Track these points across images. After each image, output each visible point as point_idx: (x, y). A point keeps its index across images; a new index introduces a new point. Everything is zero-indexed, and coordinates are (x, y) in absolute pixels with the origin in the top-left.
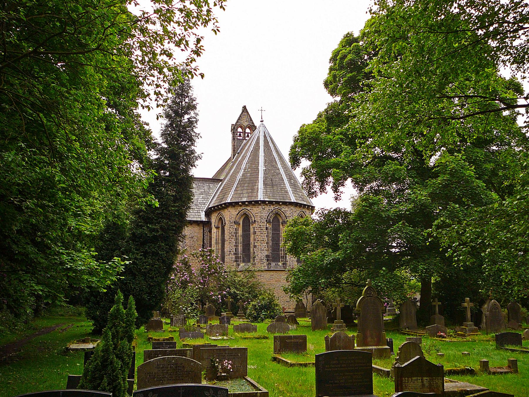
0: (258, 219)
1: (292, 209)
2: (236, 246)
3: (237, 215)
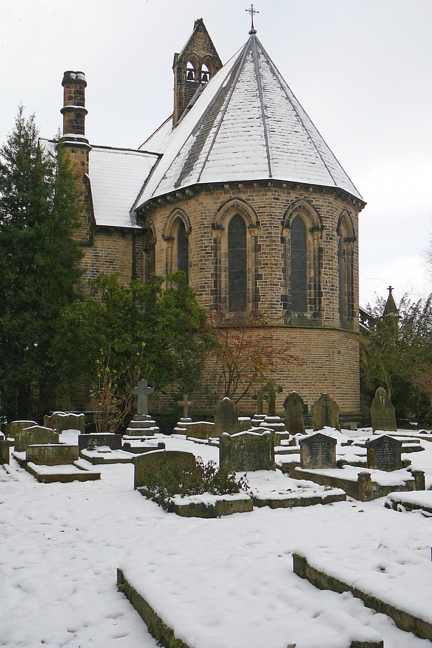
0: (264, 219)
1: (330, 203)
2: (216, 276)
3: (219, 210)
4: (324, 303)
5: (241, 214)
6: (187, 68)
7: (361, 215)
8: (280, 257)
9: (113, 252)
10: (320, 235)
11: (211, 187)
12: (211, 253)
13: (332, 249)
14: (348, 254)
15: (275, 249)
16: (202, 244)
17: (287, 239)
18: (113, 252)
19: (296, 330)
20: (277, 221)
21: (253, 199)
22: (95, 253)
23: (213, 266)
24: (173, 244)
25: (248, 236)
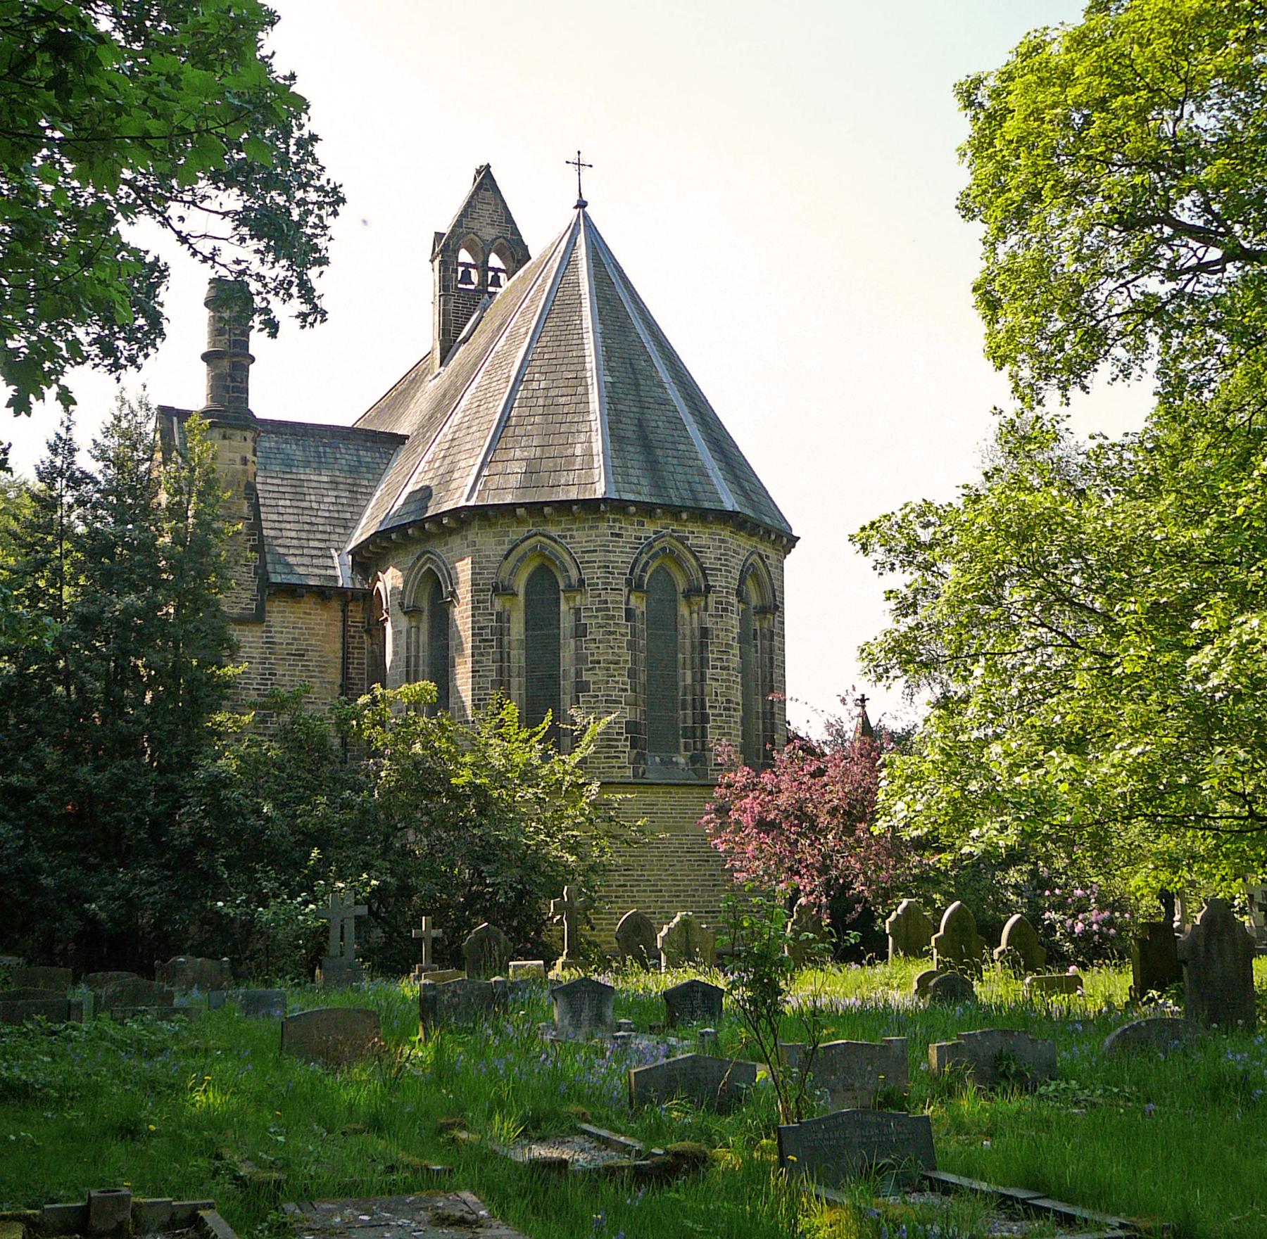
0: (594, 575)
1: (723, 541)
3: (506, 557)
4: (712, 736)
5: (547, 563)
7: (790, 562)
10: (703, 604)
11: (490, 513)
13: (727, 630)
14: (763, 637)
15: (614, 633)
17: (638, 612)
19: (656, 789)
23: (495, 666)
24: (419, 621)
25: (563, 607)
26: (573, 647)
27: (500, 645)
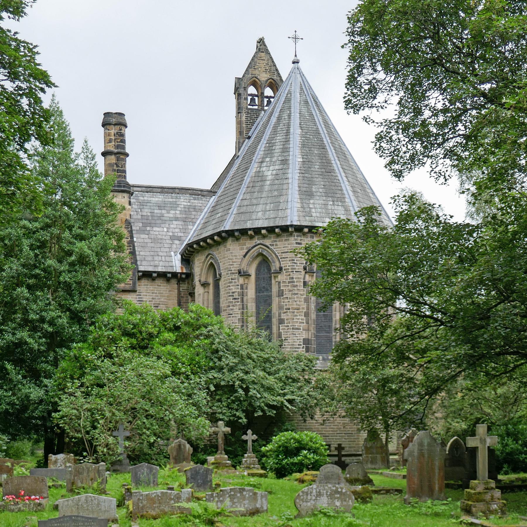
3: (245, 256)
6: (249, 93)
8: (302, 301)
9: (158, 296)
12: (238, 299)
15: (297, 294)
16: (230, 290)
18: (158, 296)
20: (299, 266)
21: (276, 245)
22: (139, 298)
24: (209, 289)
26: (277, 301)
27: (242, 301)
